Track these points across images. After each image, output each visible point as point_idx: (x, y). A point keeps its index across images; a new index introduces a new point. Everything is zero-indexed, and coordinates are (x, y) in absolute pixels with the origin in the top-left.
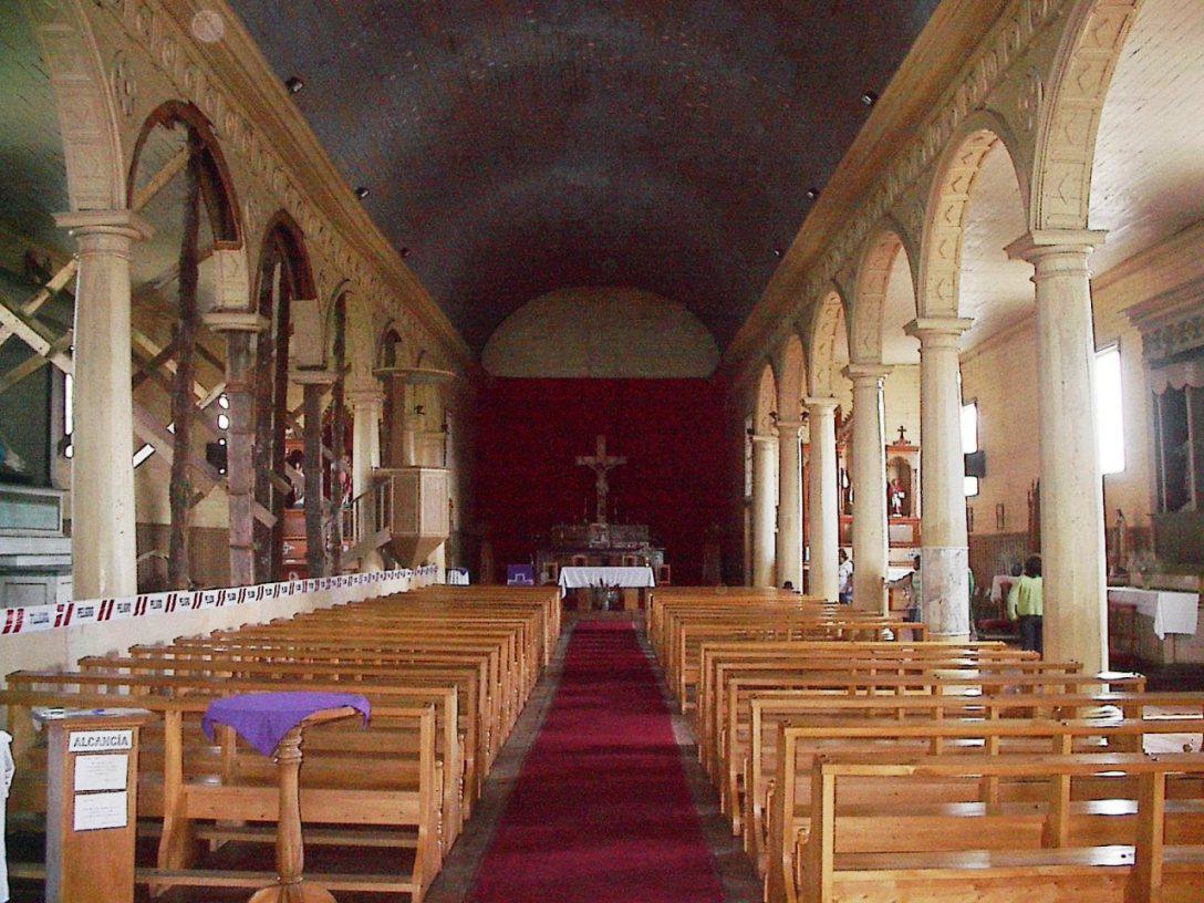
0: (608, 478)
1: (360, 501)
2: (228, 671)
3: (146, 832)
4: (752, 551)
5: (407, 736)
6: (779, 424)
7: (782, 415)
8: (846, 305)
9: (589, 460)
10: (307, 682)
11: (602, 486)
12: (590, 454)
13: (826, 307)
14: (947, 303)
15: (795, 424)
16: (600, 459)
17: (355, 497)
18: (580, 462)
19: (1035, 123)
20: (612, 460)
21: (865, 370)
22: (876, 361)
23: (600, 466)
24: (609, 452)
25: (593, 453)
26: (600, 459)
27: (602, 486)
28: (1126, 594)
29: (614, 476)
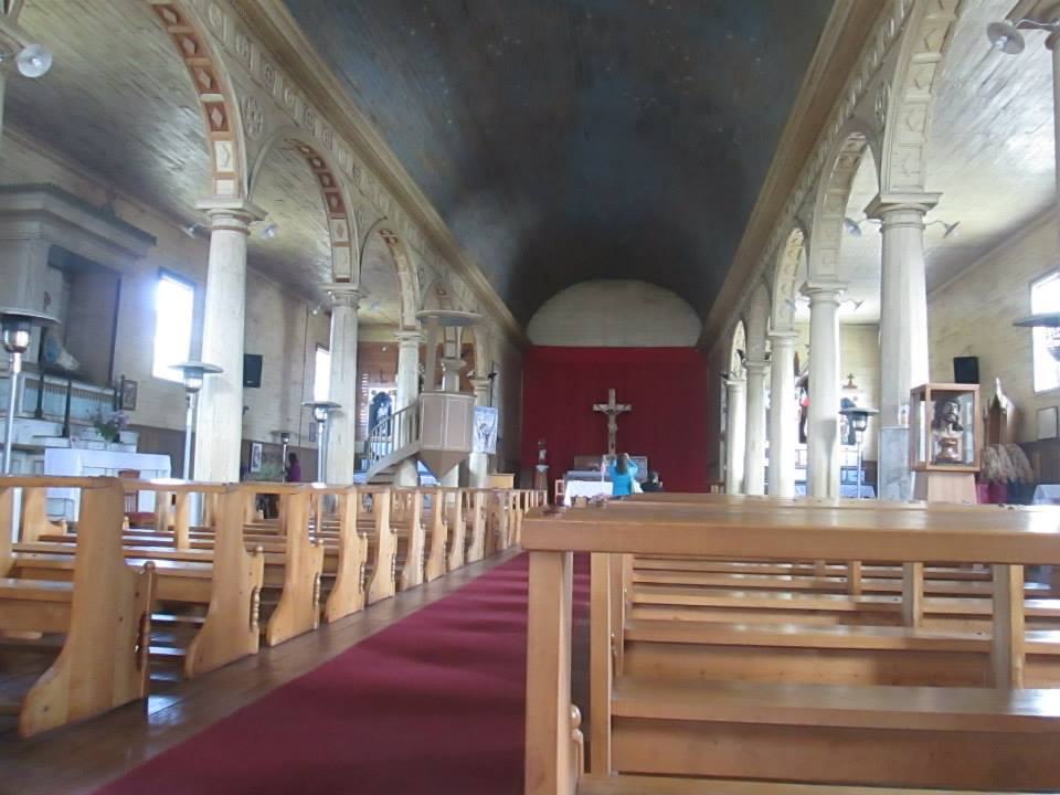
0: (618, 421)
1: (403, 414)
2: (37, 631)
3: (1003, 492)
4: (779, 478)
5: (637, 566)
6: (747, 364)
7: (750, 357)
8: (807, 235)
9: (603, 407)
10: (186, 63)
11: (613, 427)
12: (604, 403)
13: (788, 249)
14: (913, 179)
15: (762, 364)
16: (612, 406)
17: (393, 412)
18: (596, 408)
19: (885, 119)
20: (620, 407)
21: (824, 286)
22: (789, 326)
23: (610, 411)
24: (617, 402)
25: (606, 402)
26: (612, 406)
27: (613, 427)
28: (1049, 570)
29: (622, 418)
